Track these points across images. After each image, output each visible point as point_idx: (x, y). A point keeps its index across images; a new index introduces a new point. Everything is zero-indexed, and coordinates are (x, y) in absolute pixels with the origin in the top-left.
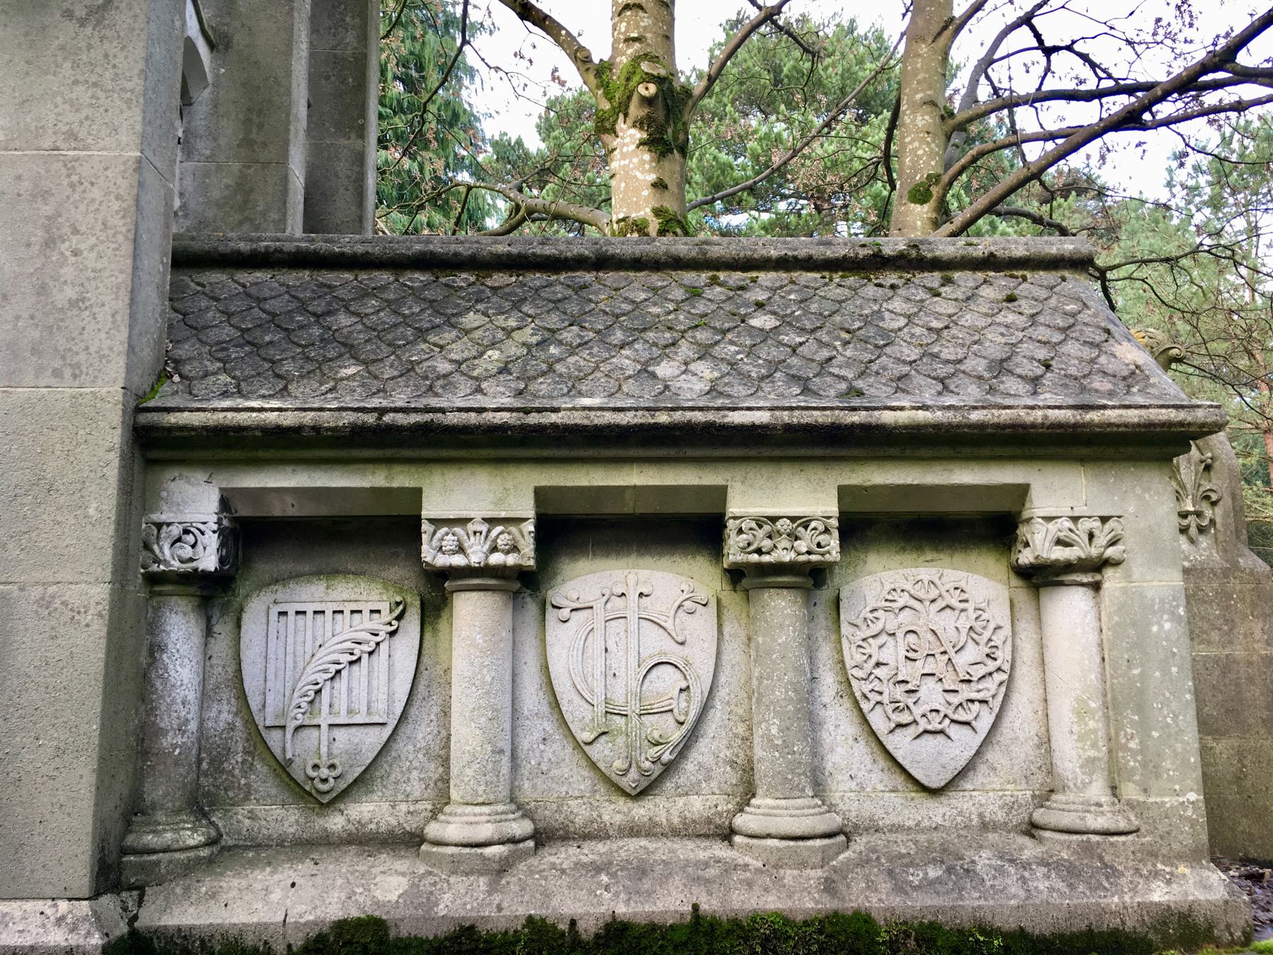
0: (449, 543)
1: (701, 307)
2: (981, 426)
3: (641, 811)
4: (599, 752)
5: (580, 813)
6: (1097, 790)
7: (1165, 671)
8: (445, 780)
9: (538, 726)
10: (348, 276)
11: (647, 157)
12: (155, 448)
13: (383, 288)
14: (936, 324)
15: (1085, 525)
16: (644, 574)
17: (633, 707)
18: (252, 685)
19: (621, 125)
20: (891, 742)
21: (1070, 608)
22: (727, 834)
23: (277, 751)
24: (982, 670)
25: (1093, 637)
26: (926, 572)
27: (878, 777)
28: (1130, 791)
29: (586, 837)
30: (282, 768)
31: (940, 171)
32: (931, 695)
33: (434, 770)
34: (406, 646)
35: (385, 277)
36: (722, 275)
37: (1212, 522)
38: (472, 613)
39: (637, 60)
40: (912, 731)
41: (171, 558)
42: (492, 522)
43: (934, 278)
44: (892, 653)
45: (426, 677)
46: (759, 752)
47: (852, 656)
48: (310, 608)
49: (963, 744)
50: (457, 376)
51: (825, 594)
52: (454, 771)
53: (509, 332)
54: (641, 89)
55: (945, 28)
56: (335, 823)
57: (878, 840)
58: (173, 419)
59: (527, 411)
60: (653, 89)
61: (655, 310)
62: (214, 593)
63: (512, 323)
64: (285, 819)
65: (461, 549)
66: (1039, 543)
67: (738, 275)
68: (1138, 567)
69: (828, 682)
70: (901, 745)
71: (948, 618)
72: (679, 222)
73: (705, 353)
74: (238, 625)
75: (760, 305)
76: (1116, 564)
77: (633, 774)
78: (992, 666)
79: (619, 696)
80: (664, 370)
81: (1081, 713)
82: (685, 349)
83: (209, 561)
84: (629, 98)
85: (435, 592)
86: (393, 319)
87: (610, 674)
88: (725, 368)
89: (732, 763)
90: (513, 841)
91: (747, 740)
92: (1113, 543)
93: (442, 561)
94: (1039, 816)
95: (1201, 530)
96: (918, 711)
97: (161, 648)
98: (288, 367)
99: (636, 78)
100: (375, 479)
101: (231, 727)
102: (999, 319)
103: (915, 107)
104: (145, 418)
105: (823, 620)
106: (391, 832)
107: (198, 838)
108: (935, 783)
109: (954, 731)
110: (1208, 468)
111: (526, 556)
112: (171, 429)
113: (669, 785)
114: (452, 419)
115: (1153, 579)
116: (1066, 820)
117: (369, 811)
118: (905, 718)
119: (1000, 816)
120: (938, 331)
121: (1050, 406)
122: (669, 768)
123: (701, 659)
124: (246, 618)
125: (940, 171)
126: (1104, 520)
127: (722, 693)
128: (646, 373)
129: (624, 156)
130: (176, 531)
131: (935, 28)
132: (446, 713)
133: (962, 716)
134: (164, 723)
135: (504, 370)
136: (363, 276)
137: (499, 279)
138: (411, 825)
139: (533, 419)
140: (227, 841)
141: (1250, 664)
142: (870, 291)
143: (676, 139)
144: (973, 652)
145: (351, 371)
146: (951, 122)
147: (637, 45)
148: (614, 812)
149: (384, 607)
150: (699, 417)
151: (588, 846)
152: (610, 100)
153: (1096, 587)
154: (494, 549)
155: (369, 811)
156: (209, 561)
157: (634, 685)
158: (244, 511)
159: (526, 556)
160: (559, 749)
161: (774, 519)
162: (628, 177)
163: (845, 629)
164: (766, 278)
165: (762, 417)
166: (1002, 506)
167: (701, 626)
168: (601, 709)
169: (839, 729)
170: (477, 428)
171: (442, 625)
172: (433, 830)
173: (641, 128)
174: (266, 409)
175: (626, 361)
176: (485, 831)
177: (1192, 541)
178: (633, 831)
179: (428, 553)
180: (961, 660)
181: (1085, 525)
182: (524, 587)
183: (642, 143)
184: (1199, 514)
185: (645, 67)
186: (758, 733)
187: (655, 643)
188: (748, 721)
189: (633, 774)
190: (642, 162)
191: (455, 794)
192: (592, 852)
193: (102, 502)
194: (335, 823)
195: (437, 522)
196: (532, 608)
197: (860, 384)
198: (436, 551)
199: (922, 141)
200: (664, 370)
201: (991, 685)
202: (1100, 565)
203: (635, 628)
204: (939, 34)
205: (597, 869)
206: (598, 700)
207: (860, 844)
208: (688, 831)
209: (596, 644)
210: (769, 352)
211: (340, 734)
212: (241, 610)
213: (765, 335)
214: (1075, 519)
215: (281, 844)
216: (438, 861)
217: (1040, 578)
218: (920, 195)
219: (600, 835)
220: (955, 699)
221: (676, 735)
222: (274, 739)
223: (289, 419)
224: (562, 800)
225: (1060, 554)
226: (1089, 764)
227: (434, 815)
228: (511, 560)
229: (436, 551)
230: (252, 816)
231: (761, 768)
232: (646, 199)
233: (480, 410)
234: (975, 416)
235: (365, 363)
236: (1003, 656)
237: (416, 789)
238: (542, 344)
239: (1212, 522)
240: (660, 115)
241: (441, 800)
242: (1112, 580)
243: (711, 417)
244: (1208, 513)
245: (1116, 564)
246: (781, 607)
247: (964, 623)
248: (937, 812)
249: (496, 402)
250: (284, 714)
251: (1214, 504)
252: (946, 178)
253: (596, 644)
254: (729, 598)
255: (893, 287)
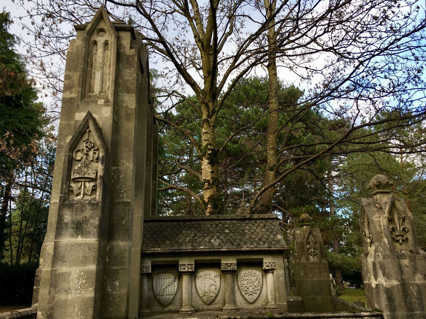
0: (183, 268)
1: (218, 229)
2: (255, 250)
3: (209, 307)
4: (204, 298)
5: (201, 307)
6: (273, 303)
7: (282, 285)
8: (182, 303)
9: (195, 295)
10: (164, 223)
11: (210, 166)
12: (144, 255)
13: (170, 226)
14: (252, 231)
15: (271, 264)
16: (210, 271)
17: (208, 291)
18: (155, 289)
19: (204, 159)
20: (245, 296)
21: (270, 276)
22: (222, 310)
23: (158, 298)
24: (258, 285)
25: (273, 280)
26: (250, 271)
27: (243, 302)
28: (277, 303)
29: (202, 311)
30: (159, 301)
31: (276, 164)
32: (251, 289)
33: (180, 301)
34: (176, 283)
35: (170, 223)
36: (221, 222)
37: (317, 253)
38: (185, 279)
39: (207, 145)
40: (248, 294)
41: (145, 271)
42: (189, 265)
43: (253, 222)
44: (245, 283)
45: (180, 287)
46: (226, 298)
47: (239, 283)
48: (163, 278)
49: (255, 296)
50: (183, 243)
51: (236, 274)
52: (183, 301)
53: (189, 234)
54: (208, 152)
55: (276, 131)
56: (166, 309)
57: (243, 311)
58: (146, 252)
59: (193, 249)
60: (211, 152)
61: (211, 229)
62: (149, 276)
63: (190, 232)
64: (158, 308)
65: (184, 269)
66: (265, 267)
67: (224, 221)
68: (278, 270)
69: (236, 287)
70: (246, 296)
71: (253, 278)
72: (217, 180)
73: (218, 238)
74: (152, 280)
75: (227, 228)
76: (275, 269)
77: (208, 301)
78: (259, 284)
79: (206, 289)
80: (212, 241)
81: (271, 291)
82: (215, 237)
83: (150, 272)
84: (206, 153)
85: (180, 276)
86: (173, 232)
87: (205, 287)
88: (221, 240)
89: (223, 300)
90: (192, 311)
91: (225, 296)
92: (275, 266)
93: (182, 270)
94: (266, 307)
95: (315, 255)
96: (249, 291)
97: (143, 284)
98: (159, 242)
99: (207, 149)
100: (173, 259)
101: (151, 295)
102: (262, 230)
103: (270, 149)
104: (143, 252)
105: (235, 278)
106: (174, 311)
107: (149, 311)
108: (251, 302)
109: (254, 294)
110: (316, 243)
111: (193, 270)
112: (146, 253)
113: (214, 303)
114: (183, 251)
115: (280, 272)
116: (269, 307)
117: (171, 307)
118: (247, 292)
119: (261, 307)
120: (252, 233)
121: (265, 247)
122: (214, 300)
123: (218, 284)
124: (154, 279)
125: (276, 164)
126: (273, 263)
127: (221, 289)
128: (210, 242)
129: (204, 165)
130: (146, 267)
131: (274, 132)
132: (182, 293)
133: (255, 292)
134: (144, 295)
135: (190, 241)
136: (167, 223)
137: (187, 223)
138: (177, 309)
139: (194, 250)
140: (151, 312)
141: (324, 281)
142: (244, 225)
143: (216, 161)
144: (256, 283)
145: (168, 242)
146: (278, 152)
147: (207, 141)
148: (206, 307)
149: (173, 277)
150: (217, 249)
151: (202, 312)
152: (202, 153)
153: (273, 273)
154: (189, 269)
155: (171, 307)
156: (150, 272)
157: (208, 288)
158: (154, 264)
159: (193, 270)
160: (198, 298)
161: (228, 264)
162: (205, 170)
163: (238, 279)
164: (228, 222)
165: (226, 249)
166: (260, 261)
167: (218, 279)
168: (204, 292)
169: (238, 294)
170: (187, 252)
171: (181, 280)
172: (181, 310)
173: (208, 160)
174: (158, 250)
175: (207, 239)
176: (188, 310)
177: (313, 257)
178: (209, 310)
179: (180, 270)
180: (255, 284)
181: (271, 264)
182: (193, 275)
183: (208, 163)
184: (314, 252)
185: (209, 147)
186: (226, 295)
187: (211, 282)
188: (225, 293)
189: (208, 301)
190: (209, 167)
191: (183, 305)
192: (202, 313)
193: (138, 264)
194: (166, 309)
195: (181, 265)
196: (194, 277)
197: (240, 243)
198: (181, 269)
199: (272, 157)
200: (212, 241)
201: (259, 287)
202: (273, 270)
203: (209, 281)
204: (275, 133)
205: (203, 315)
206: (203, 290)
207: (240, 311)
208: (217, 310)
209: (203, 282)
210: (227, 237)
211: (167, 296)
212: (153, 278)
213: (227, 234)
214: (269, 263)
215: (159, 312)
216: (182, 314)
217: (266, 272)
218: (271, 169)
219: (204, 311)
220: (254, 290)
221: (215, 296)
222: (158, 297)
223: (162, 251)
224: (198, 305)
225: (267, 268)
226: (272, 299)
227: (180, 308)
228: (191, 270)
229: (181, 269)
230: (155, 308)
231: (226, 300)
232: (209, 175)
233: (187, 249)
234: (255, 249)
235: (170, 241)
236: (261, 283)
237: (178, 304)
238: (195, 236)
239: (317, 253)
240: (212, 157)
241: (181, 306)
242: (275, 272)
243: (219, 250)
244: (316, 252)
245: (275, 269)
246: (229, 276)
247: (255, 278)
248: (252, 307)
249: (189, 248)
250: (159, 293)
251: (317, 250)
252: (277, 166)
253: (203, 282)
254: (222, 275)
255: (247, 224)
